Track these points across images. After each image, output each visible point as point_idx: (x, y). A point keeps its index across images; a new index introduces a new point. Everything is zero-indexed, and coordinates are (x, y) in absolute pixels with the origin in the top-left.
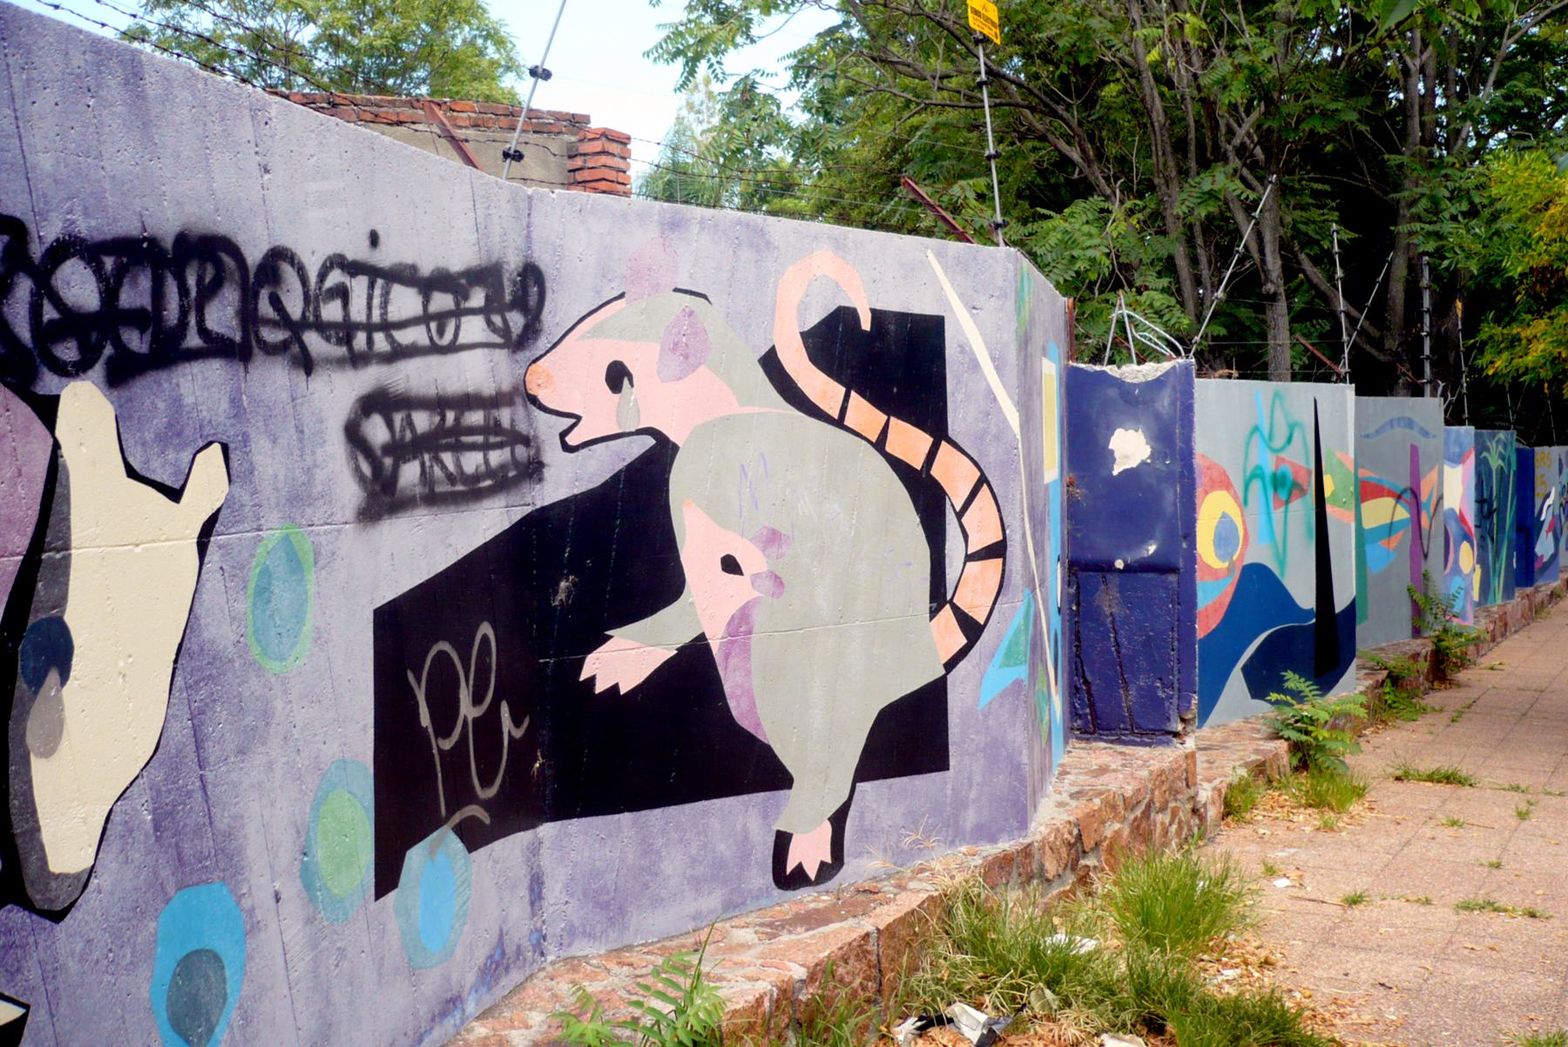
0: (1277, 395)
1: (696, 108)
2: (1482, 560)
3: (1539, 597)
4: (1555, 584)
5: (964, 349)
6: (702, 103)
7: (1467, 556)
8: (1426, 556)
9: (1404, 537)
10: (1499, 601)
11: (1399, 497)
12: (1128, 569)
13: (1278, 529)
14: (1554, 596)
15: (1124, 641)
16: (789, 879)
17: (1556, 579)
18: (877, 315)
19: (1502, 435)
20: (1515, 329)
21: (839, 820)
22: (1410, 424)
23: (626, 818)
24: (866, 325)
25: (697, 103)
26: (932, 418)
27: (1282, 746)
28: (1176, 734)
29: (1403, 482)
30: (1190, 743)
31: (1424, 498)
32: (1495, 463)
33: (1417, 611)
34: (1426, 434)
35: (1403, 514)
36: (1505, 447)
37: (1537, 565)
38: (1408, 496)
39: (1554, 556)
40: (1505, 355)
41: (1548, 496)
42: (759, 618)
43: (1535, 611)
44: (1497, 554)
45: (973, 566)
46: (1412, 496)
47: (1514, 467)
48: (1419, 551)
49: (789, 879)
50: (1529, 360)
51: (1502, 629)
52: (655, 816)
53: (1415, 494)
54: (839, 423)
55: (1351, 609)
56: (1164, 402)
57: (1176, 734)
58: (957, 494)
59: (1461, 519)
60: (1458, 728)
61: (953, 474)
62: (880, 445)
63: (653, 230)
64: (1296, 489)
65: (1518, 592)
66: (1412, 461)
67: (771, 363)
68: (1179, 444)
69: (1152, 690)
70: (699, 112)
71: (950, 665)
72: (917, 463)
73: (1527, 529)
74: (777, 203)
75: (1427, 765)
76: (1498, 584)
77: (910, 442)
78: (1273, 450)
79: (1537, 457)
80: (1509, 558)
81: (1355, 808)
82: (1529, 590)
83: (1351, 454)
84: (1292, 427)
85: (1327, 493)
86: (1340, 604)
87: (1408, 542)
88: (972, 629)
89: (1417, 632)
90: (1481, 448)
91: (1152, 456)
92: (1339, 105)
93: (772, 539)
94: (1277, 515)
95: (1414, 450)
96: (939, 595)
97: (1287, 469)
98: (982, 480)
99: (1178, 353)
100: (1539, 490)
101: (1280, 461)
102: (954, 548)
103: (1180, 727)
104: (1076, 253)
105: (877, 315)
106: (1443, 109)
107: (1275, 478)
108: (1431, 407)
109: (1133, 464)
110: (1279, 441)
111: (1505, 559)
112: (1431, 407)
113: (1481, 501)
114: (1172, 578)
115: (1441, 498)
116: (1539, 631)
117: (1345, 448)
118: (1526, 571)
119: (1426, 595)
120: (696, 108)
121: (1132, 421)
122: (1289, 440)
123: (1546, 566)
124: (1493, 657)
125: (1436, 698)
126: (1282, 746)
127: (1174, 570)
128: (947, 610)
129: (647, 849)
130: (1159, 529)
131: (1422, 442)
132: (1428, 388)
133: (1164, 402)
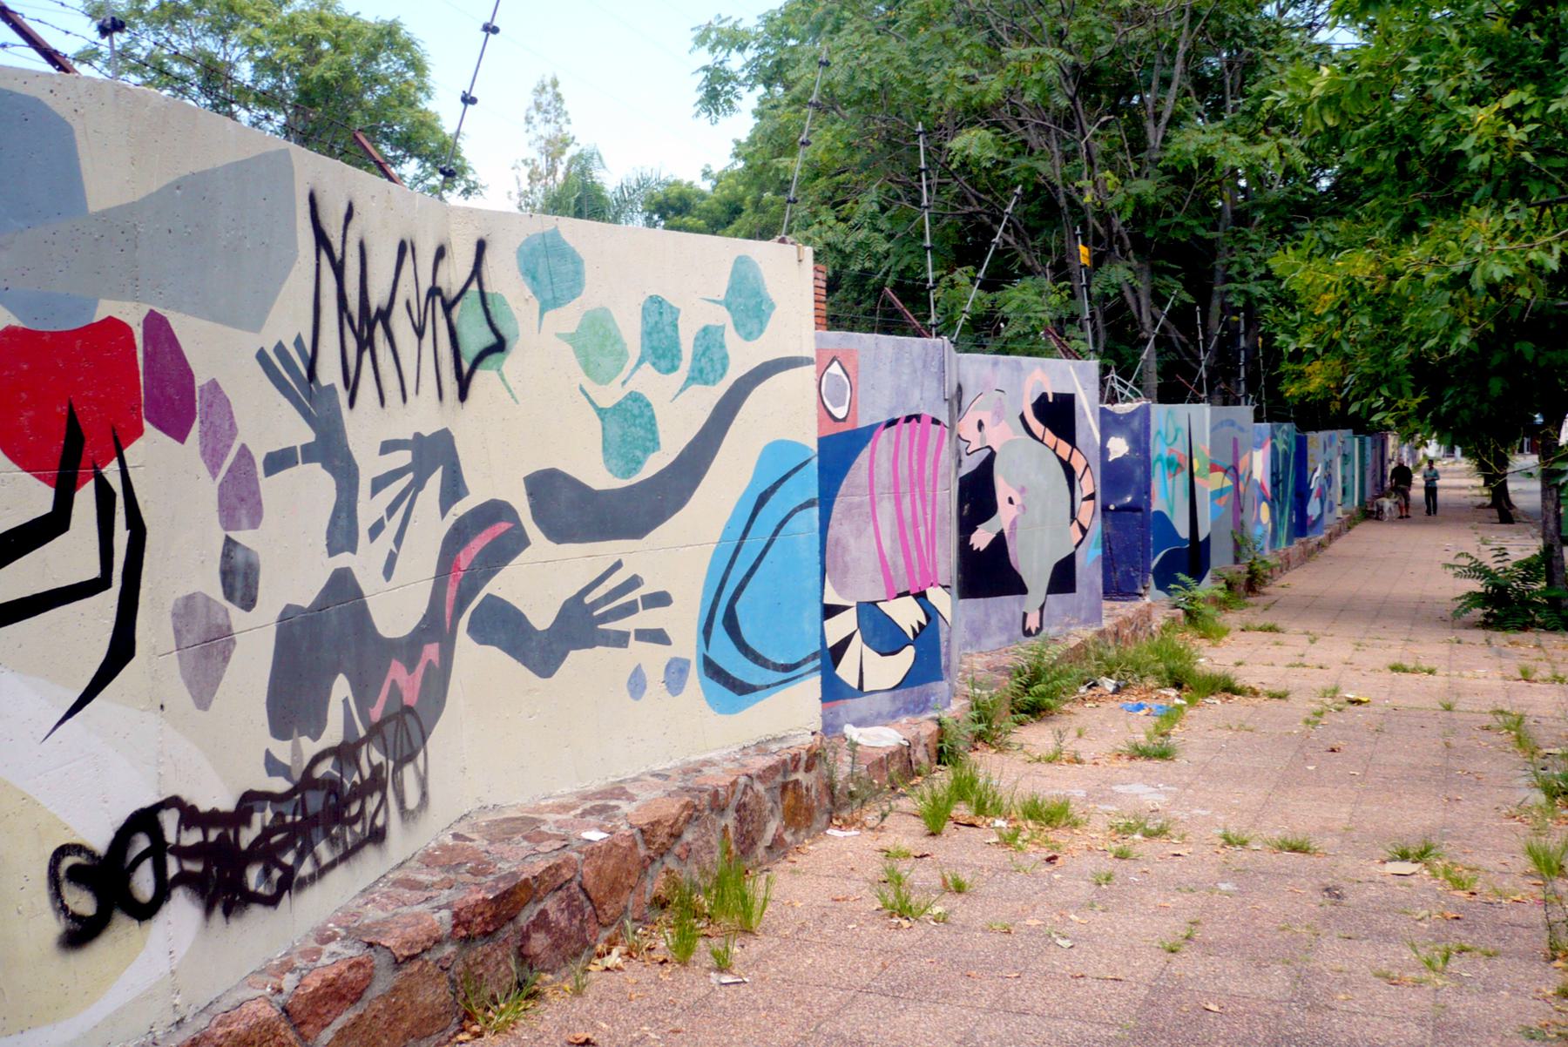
0: (1169, 412)
1: (544, 107)
2: (1273, 518)
3: (1310, 546)
4: (1321, 537)
5: (1082, 408)
6: (549, 105)
7: (1265, 511)
8: (1242, 511)
9: (1228, 498)
10: (1283, 545)
11: (1226, 472)
12: (1117, 509)
13: (1170, 490)
14: (1320, 546)
15: (1114, 547)
16: (1027, 633)
17: (1321, 533)
18: (1055, 395)
19: (1286, 426)
20: (1303, 367)
21: (1042, 609)
22: (1232, 423)
23: (981, 600)
24: (1051, 400)
25: (545, 103)
26: (1071, 440)
27: (1180, 611)
28: (1141, 595)
29: (1229, 462)
30: (1148, 600)
31: (1241, 472)
32: (1281, 447)
33: (1237, 547)
34: (1241, 429)
35: (1228, 483)
36: (1288, 435)
37: (1309, 523)
38: (1231, 471)
39: (1321, 516)
40: (1296, 385)
41: (1315, 470)
42: (1019, 523)
43: (1308, 555)
44: (1282, 513)
45: (1085, 503)
46: (1233, 471)
47: (1294, 449)
48: (1238, 508)
49: (1027, 633)
50: (1311, 388)
51: (1287, 565)
52: (990, 600)
53: (1236, 469)
54: (1042, 441)
55: (1208, 539)
56: (1136, 424)
57: (1141, 595)
58: (1079, 471)
59: (1262, 486)
60: (1266, 613)
61: (1078, 463)
62: (1054, 450)
63: (990, 366)
64: (1180, 467)
65: (1296, 541)
66: (750, 373)
67: (1022, 417)
68: (1143, 445)
69: (1128, 573)
70: (546, 112)
71: (1077, 546)
72: (1066, 459)
73: (1302, 494)
74: (678, 220)
75: (1258, 623)
76: (1283, 534)
77: (1064, 448)
78: (1168, 445)
79: (1309, 440)
80: (1290, 516)
81: (1226, 639)
82: (1303, 539)
83: (1208, 447)
84: (1177, 430)
85: (1195, 470)
86: (1202, 537)
87: (1231, 502)
88: (1084, 531)
89: (1237, 560)
90: (1273, 436)
91: (1130, 451)
92: (1195, 223)
93: (1022, 490)
94: (1169, 482)
95: (1235, 441)
96: (1073, 517)
97: (1176, 457)
98: (1087, 466)
99: (1137, 395)
100: (1310, 465)
101: (1171, 451)
102: (1078, 496)
103: (1142, 591)
104: (1031, 315)
105: (1055, 395)
106: (1244, 191)
107: (1168, 460)
108: (1245, 412)
109: (1119, 455)
110: (1170, 440)
111: (1288, 518)
112: (1245, 412)
113: (1274, 474)
114: (1139, 514)
115: (1251, 473)
116: (1311, 567)
117: (1204, 444)
118: (1301, 526)
119: (1243, 537)
120: (544, 107)
121: (1119, 434)
122: (1175, 439)
123: (1315, 523)
124: (1284, 580)
125: (1252, 600)
126: (1180, 611)
127: (1140, 510)
128: (1075, 522)
129: (987, 615)
130: (1133, 489)
131: (1240, 436)
132: (1243, 400)
133: (1136, 424)
